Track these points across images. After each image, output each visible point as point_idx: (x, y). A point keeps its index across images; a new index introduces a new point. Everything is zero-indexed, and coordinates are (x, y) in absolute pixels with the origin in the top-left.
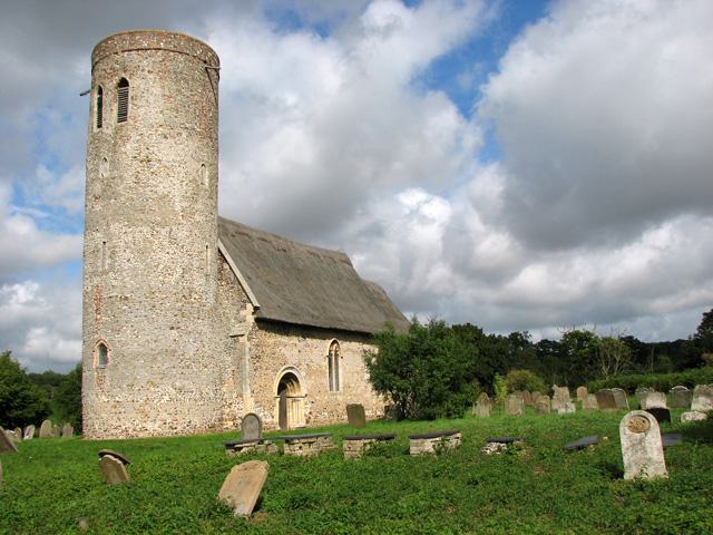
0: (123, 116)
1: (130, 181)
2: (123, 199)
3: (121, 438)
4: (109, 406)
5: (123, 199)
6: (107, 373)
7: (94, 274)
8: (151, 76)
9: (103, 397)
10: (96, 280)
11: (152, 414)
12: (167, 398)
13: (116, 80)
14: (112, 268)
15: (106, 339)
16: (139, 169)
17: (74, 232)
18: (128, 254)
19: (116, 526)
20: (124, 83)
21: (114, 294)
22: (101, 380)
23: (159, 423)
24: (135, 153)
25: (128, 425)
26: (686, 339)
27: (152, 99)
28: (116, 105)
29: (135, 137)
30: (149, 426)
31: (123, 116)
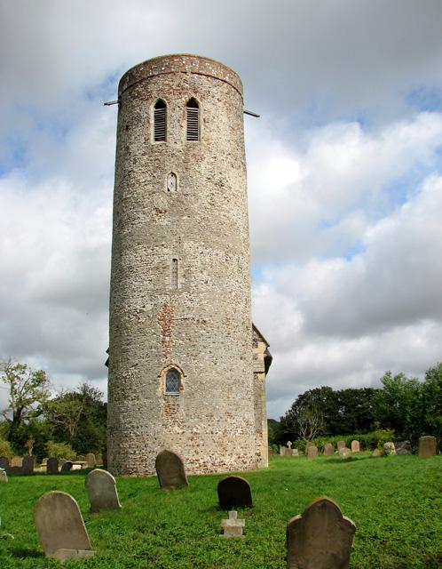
0: (193, 133)
1: (206, 201)
2: (197, 217)
3: (198, 473)
4: (185, 439)
5: (197, 217)
6: (182, 401)
7: (162, 292)
8: (220, 104)
9: (176, 428)
10: (161, 300)
11: (229, 448)
12: (240, 430)
13: (185, 98)
14: (186, 288)
15: (177, 361)
16: (213, 192)
17: (189, 476)
18: (205, 276)
19: (172, 190)
20: (192, 103)
21: (190, 316)
22: (171, 410)
23: (235, 457)
24: (209, 175)
25: (207, 458)
26: (381, 386)
27: (222, 127)
28: (186, 122)
29: (208, 158)
30: (227, 460)
31: (193, 133)
